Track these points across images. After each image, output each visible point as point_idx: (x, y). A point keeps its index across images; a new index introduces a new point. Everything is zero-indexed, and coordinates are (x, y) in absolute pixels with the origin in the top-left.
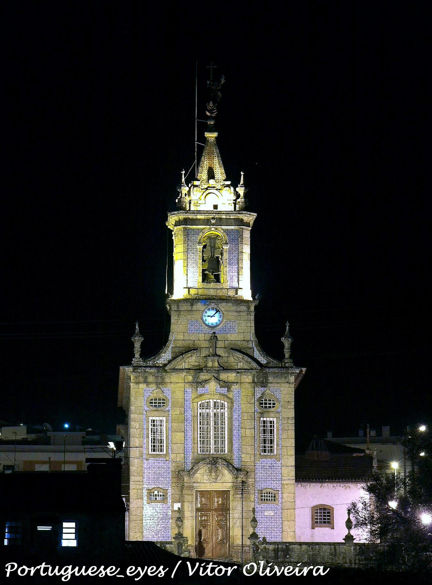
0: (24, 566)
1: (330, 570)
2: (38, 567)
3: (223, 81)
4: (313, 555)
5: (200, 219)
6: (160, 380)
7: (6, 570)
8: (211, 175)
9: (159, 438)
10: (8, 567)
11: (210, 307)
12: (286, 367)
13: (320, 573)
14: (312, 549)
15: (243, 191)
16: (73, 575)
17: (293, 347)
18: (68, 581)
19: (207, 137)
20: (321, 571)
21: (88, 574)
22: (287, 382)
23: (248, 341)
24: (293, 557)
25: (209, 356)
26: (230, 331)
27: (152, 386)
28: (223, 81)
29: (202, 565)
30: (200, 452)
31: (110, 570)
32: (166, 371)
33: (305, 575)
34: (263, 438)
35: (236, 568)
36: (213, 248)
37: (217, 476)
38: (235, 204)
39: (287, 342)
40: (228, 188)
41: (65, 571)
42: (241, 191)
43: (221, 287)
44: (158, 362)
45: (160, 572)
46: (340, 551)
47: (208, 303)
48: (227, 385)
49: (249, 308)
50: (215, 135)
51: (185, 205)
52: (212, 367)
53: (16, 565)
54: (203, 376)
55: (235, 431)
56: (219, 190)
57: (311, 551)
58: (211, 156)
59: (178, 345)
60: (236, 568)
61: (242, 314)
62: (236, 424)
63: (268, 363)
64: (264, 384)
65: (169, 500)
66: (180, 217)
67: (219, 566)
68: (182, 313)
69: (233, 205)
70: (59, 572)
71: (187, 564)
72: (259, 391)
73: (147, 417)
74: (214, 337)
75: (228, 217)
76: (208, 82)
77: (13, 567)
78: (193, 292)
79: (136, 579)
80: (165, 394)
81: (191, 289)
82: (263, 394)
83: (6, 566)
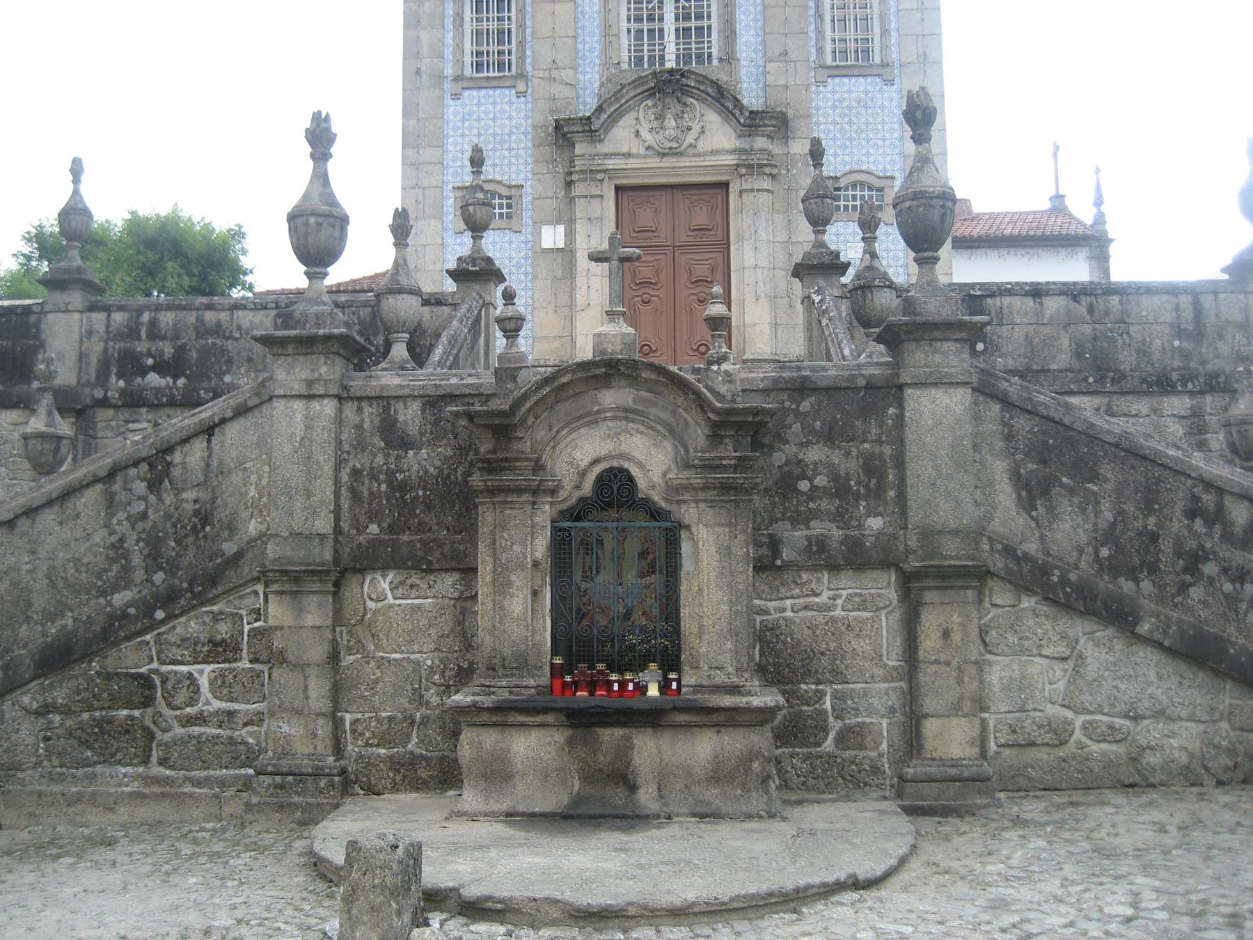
4: (1095, 338)
14: (1091, 310)
24: (1004, 350)
46: (1217, 316)
57: (1088, 318)
65: (527, 218)
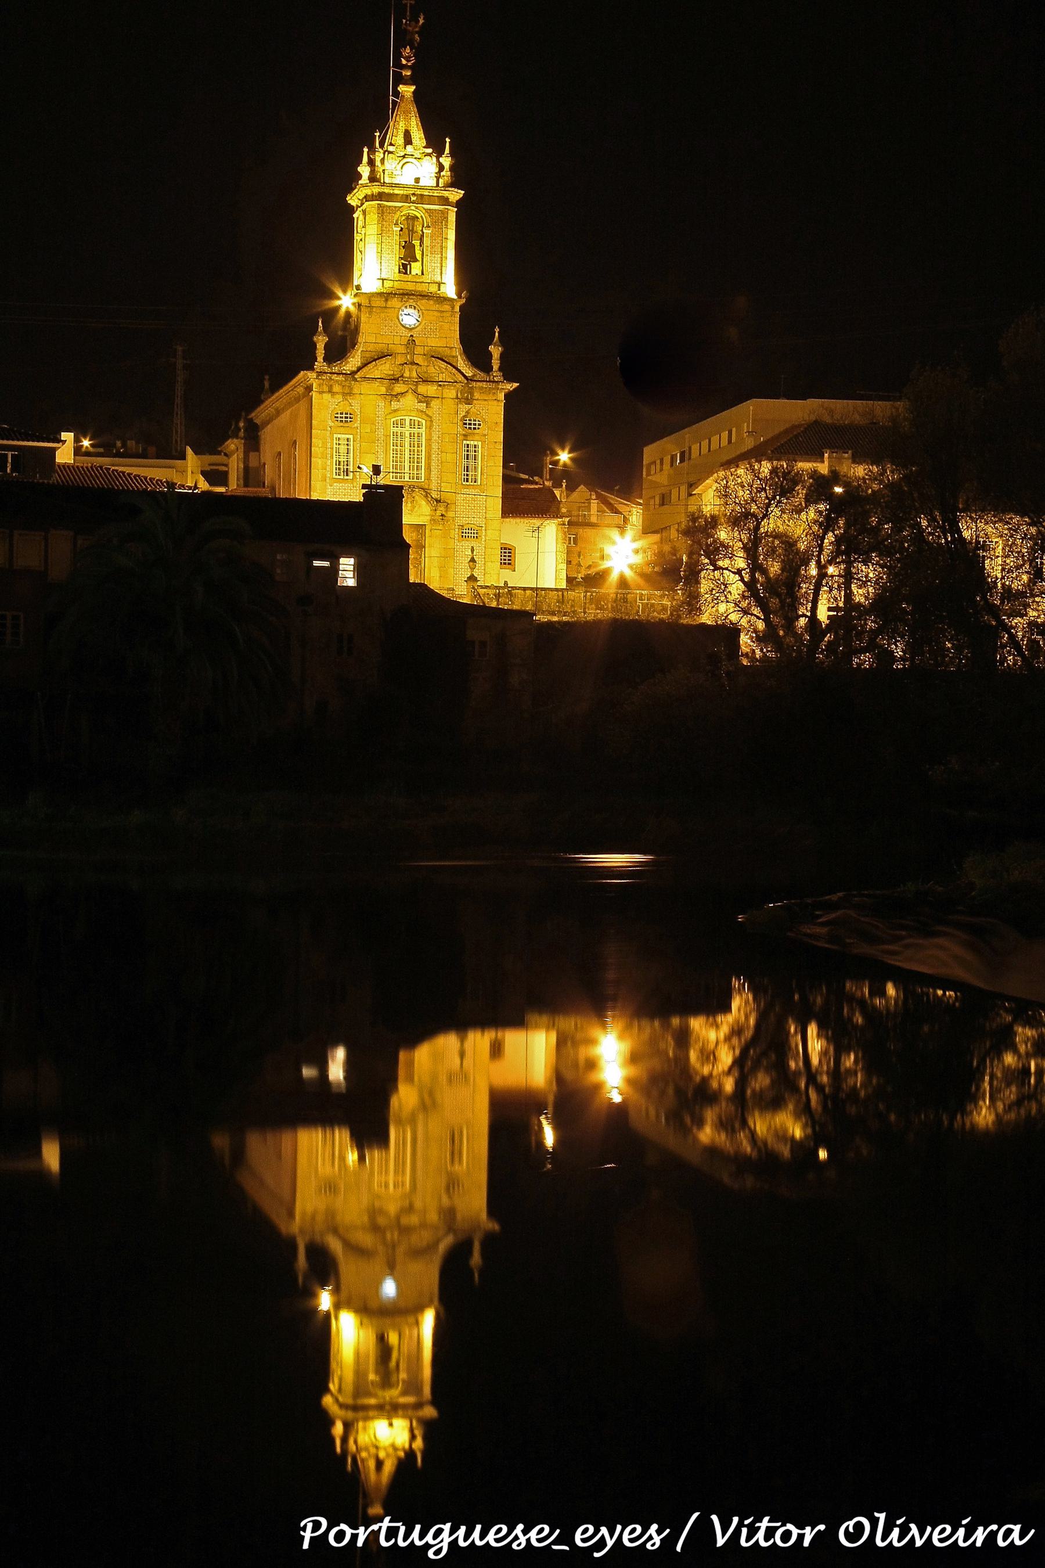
0: (341, 1525)
1: (1035, 1533)
2: (375, 1527)
3: (421, 21)
5: (397, 195)
6: (347, 390)
7: (302, 1533)
8: (408, 140)
9: (345, 460)
10: (305, 1525)
11: (408, 304)
12: (494, 382)
13: (1013, 1540)
15: (449, 163)
16: (454, 1544)
17: (502, 356)
18: (443, 1557)
19: (402, 91)
20: (1015, 1535)
21: (488, 1542)
22: (495, 399)
23: (451, 348)
25: (406, 363)
26: (431, 335)
27: (337, 396)
28: (421, 21)
29: (747, 1522)
30: (393, 478)
31: (538, 1534)
32: (355, 380)
33: (979, 1544)
34: (466, 465)
35: (822, 1530)
36: (412, 231)
37: (414, 507)
38: (438, 179)
39: (496, 351)
40: (429, 157)
41: (435, 1537)
42: (446, 161)
43: (421, 280)
44: (345, 368)
45: (650, 1538)
47: (405, 300)
48: (427, 400)
49: (453, 308)
50: (413, 88)
51: (380, 176)
52: (410, 378)
53: (324, 1522)
54: (399, 388)
55: (434, 455)
56: (419, 159)
58: (407, 116)
59: (369, 349)
60: (822, 1530)
61: (445, 314)
62: (435, 446)
63: (474, 375)
64: (469, 401)
66: (374, 191)
67: (784, 1525)
68: (374, 310)
69: (435, 179)
70: (421, 1538)
71: (712, 1521)
72: (464, 408)
73: (332, 434)
74: (411, 342)
75: (431, 194)
76: (404, 21)
77: (317, 1526)
78: (388, 284)
79: (596, 1555)
80: (353, 407)
81: (385, 281)
82: (468, 412)
83: (302, 1524)
